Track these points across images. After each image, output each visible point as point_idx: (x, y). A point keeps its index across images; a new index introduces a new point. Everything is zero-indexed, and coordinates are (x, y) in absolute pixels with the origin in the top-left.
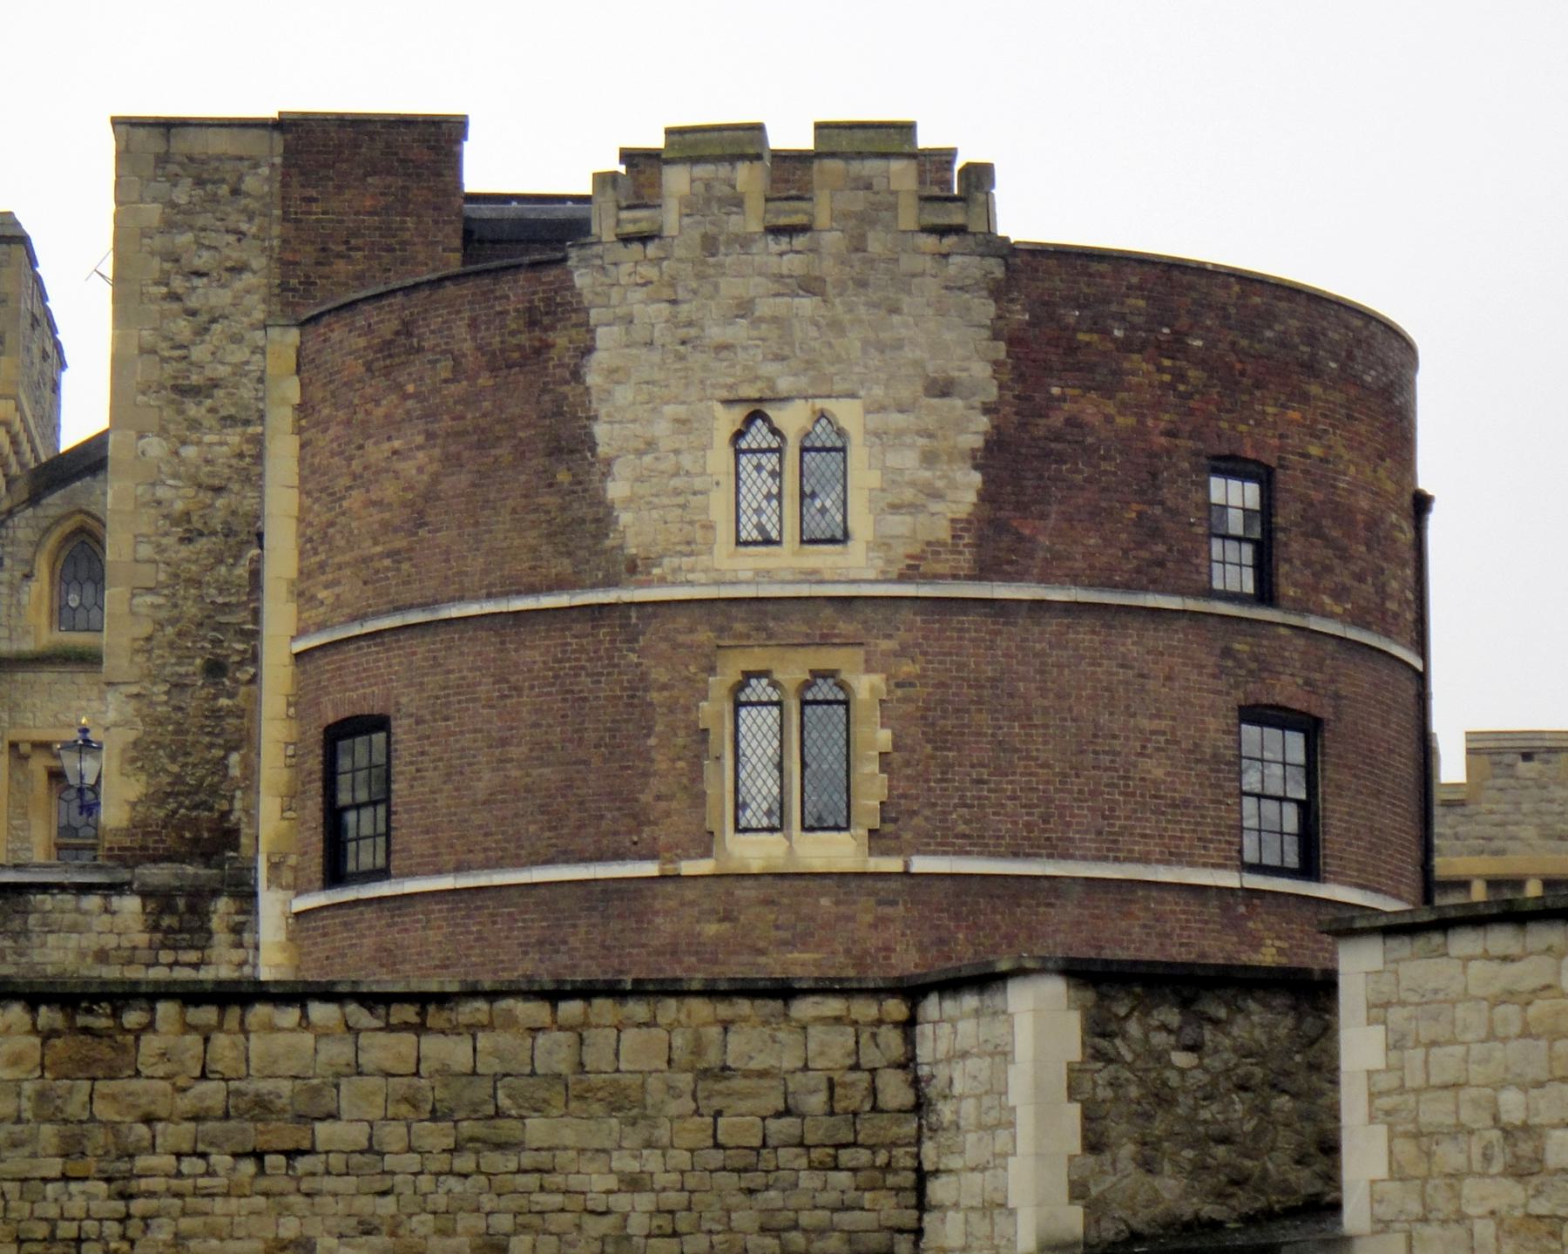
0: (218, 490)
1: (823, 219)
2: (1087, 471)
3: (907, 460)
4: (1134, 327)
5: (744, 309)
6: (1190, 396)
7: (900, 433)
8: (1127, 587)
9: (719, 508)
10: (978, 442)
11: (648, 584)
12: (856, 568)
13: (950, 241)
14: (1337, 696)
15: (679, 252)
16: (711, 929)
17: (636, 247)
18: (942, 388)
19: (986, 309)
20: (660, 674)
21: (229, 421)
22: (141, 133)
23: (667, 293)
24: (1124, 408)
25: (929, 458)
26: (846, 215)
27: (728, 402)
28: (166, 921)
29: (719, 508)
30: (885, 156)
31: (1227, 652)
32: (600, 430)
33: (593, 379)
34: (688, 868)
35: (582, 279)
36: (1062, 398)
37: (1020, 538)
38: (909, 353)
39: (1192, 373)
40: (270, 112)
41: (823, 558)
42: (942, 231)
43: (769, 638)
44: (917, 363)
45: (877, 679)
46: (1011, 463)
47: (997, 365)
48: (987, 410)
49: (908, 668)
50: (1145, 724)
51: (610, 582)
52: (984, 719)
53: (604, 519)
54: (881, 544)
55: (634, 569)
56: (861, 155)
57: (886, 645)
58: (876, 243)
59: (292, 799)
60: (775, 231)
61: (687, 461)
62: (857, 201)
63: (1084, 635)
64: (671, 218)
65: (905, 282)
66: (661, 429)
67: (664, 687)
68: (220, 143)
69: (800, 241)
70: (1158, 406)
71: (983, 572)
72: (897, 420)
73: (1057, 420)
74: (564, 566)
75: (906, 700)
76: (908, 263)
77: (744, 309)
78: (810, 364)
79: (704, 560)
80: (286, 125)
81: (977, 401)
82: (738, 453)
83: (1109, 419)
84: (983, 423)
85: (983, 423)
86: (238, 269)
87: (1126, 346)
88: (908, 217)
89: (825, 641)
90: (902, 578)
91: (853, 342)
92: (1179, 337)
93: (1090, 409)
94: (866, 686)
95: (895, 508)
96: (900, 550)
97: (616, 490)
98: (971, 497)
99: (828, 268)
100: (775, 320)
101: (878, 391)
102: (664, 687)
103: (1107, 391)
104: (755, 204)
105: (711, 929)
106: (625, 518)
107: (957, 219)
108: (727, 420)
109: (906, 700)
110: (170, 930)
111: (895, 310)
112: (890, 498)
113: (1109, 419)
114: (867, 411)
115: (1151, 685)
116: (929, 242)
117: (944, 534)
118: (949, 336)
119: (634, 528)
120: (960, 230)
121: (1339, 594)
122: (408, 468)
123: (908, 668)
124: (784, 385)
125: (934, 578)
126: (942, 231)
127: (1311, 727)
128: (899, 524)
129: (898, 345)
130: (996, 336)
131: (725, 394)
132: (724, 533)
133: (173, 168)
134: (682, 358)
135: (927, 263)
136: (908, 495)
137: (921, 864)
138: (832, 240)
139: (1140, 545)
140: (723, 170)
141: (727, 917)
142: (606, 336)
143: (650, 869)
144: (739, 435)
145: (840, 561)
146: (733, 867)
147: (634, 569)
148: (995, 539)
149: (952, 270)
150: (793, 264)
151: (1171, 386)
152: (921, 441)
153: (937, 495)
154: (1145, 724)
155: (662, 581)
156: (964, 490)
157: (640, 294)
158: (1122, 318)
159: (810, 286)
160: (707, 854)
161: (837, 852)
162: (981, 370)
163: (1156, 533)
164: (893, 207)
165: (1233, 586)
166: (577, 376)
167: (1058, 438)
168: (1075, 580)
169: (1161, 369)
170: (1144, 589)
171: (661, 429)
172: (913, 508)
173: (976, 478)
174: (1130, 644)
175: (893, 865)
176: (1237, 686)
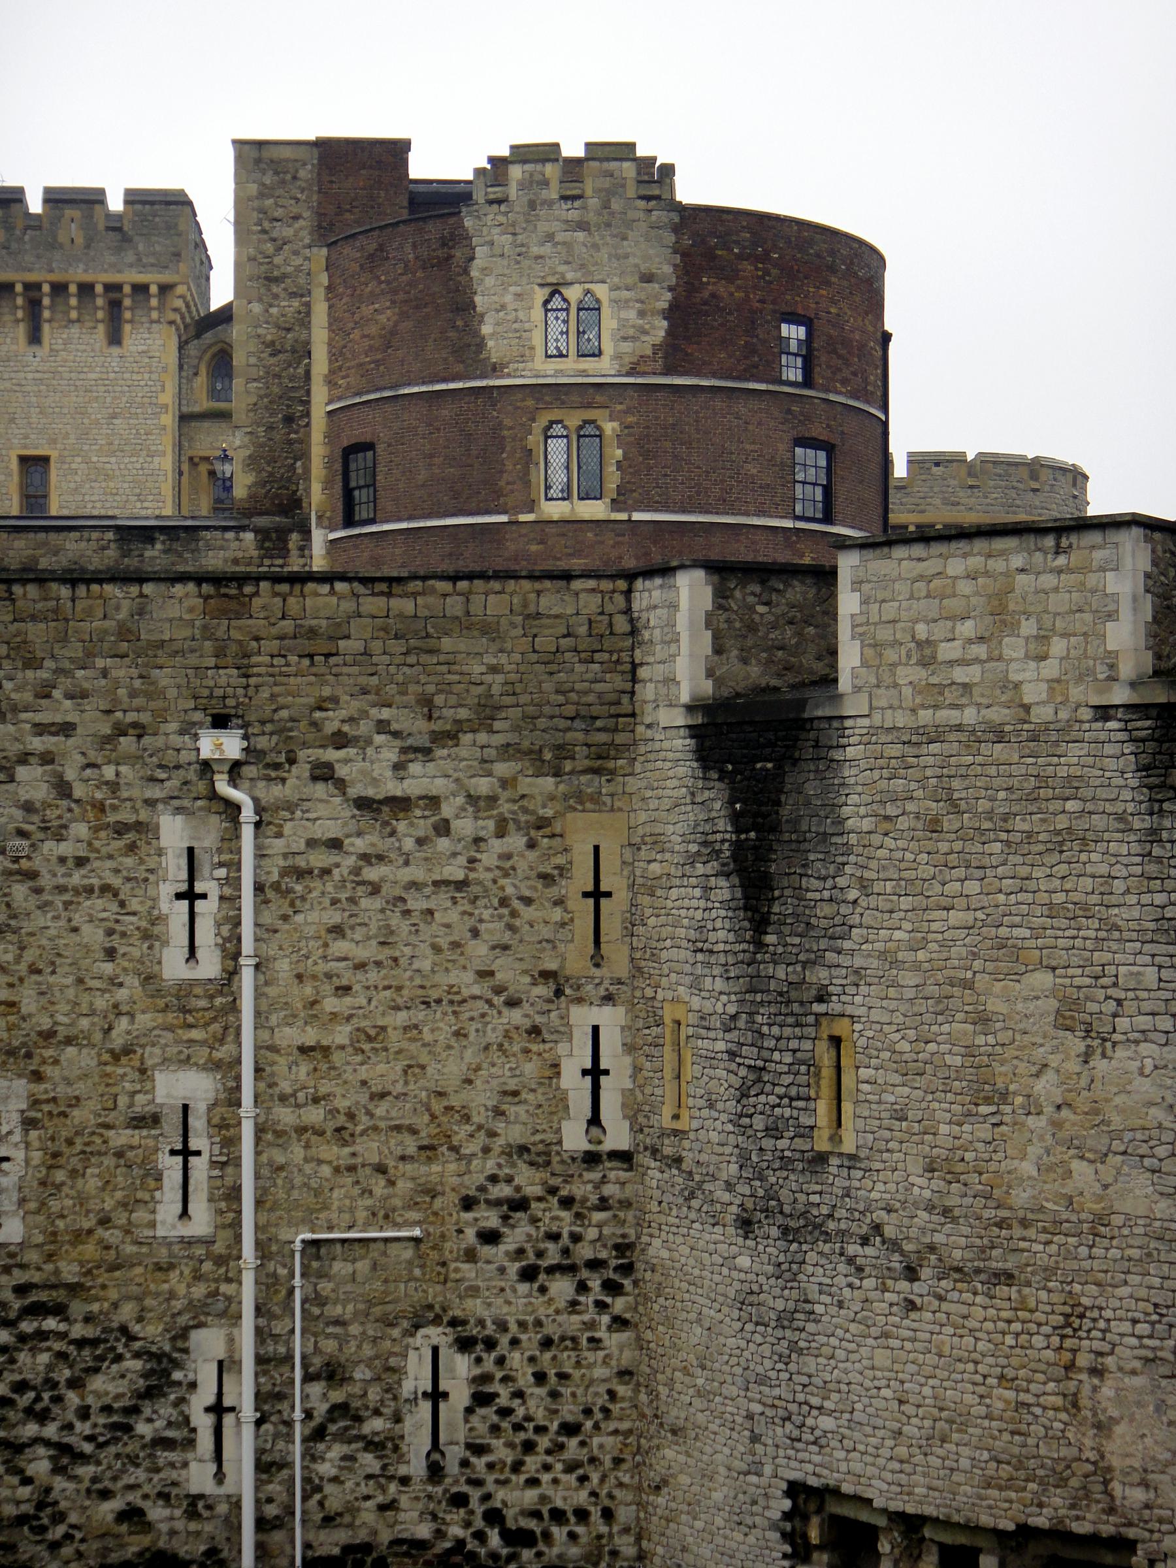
0: (288, 330)
1: (589, 192)
2: (720, 321)
3: (631, 314)
4: (745, 248)
5: (550, 237)
6: (771, 282)
7: (627, 301)
8: (738, 378)
9: (537, 339)
10: (666, 305)
11: (498, 377)
12: (605, 369)
13: (653, 203)
14: (843, 433)
15: (517, 209)
16: (534, 548)
17: (495, 206)
18: (648, 278)
19: (670, 238)
20: (508, 422)
21: (293, 295)
22: (247, 147)
23: (511, 229)
24: (739, 288)
25: (642, 314)
26: (600, 190)
27: (541, 285)
28: (267, 544)
29: (537, 339)
30: (621, 160)
31: (789, 411)
32: (478, 299)
33: (474, 273)
34: (523, 518)
35: (468, 223)
36: (708, 283)
37: (687, 354)
38: (631, 260)
39: (775, 272)
40: (311, 136)
41: (588, 364)
42: (648, 198)
43: (563, 405)
44: (636, 266)
45: (615, 424)
46: (682, 315)
47: (675, 266)
48: (670, 289)
49: (631, 419)
50: (748, 447)
51: (483, 376)
52: (668, 444)
53: (481, 345)
54: (618, 357)
55: (495, 369)
56: (608, 160)
57: (619, 407)
58: (616, 205)
59: (327, 484)
60: (564, 198)
61: (521, 315)
62: (607, 183)
63: (718, 403)
64: (513, 191)
65: (630, 224)
66: (508, 298)
67: (511, 428)
68: (287, 153)
69: (577, 204)
70: (755, 287)
71: (668, 371)
72: (626, 294)
73: (706, 294)
74: (460, 368)
75: (629, 435)
76: (631, 215)
77: (550, 237)
78: (583, 266)
79: (530, 365)
80: (323, 145)
81: (665, 285)
82: (547, 311)
83: (732, 294)
84: (669, 296)
85: (669, 296)
86: (296, 218)
87: (740, 257)
88: (631, 192)
89: (589, 406)
90: (628, 374)
91: (604, 255)
92: (767, 253)
93: (722, 289)
94: (610, 428)
95: (625, 339)
96: (627, 360)
97: (486, 329)
98: (663, 333)
99: (591, 217)
100: (564, 243)
101: (616, 280)
102: (511, 428)
103: (730, 280)
104: (555, 184)
105: (534, 548)
106: (490, 344)
107: (657, 192)
108: (541, 295)
109: (629, 435)
110: (267, 549)
111: (625, 238)
112: (622, 333)
113: (732, 294)
114: (611, 290)
115: (750, 427)
116: (642, 204)
117: (649, 352)
118: (651, 252)
119: (495, 349)
120: (658, 198)
121: (844, 382)
122: (383, 318)
123: (631, 419)
124: (570, 276)
125: (643, 374)
126: (648, 198)
127: (829, 448)
128: (626, 347)
129: (626, 256)
130: (675, 252)
131: (539, 281)
132: (540, 352)
133: (263, 166)
134: (518, 263)
135: (641, 215)
136: (631, 332)
137: (636, 516)
138: (594, 202)
139: (746, 358)
140: (539, 167)
141: (541, 542)
142: (480, 252)
143: (504, 518)
144: (546, 302)
145: (597, 365)
146: (545, 517)
147: (495, 369)
148: (674, 354)
149: (653, 218)
150: (574, 215)
151: (763, 277)
152: (638, 305)
153: (646, 333)
154: (748, 447)
155: (509, 375)
156: (659, 329)
157: (497, 230)
158: (737, 242)
159: (582, 226)
160: (531, 511)
161: (595, 510)
162: (668, 269)
163: (754, 352)
164: (624, 186)
165: (792, 378)
166: (466, 271)
167: (705, 303)
168: (714, 375)
169: (757, 269)
170: (747, 380)
171: (508, 298)
172: (634, 339)
173: (665, 323)
174: (741, 407)
175: (623, 516)
176: (793, 428)
